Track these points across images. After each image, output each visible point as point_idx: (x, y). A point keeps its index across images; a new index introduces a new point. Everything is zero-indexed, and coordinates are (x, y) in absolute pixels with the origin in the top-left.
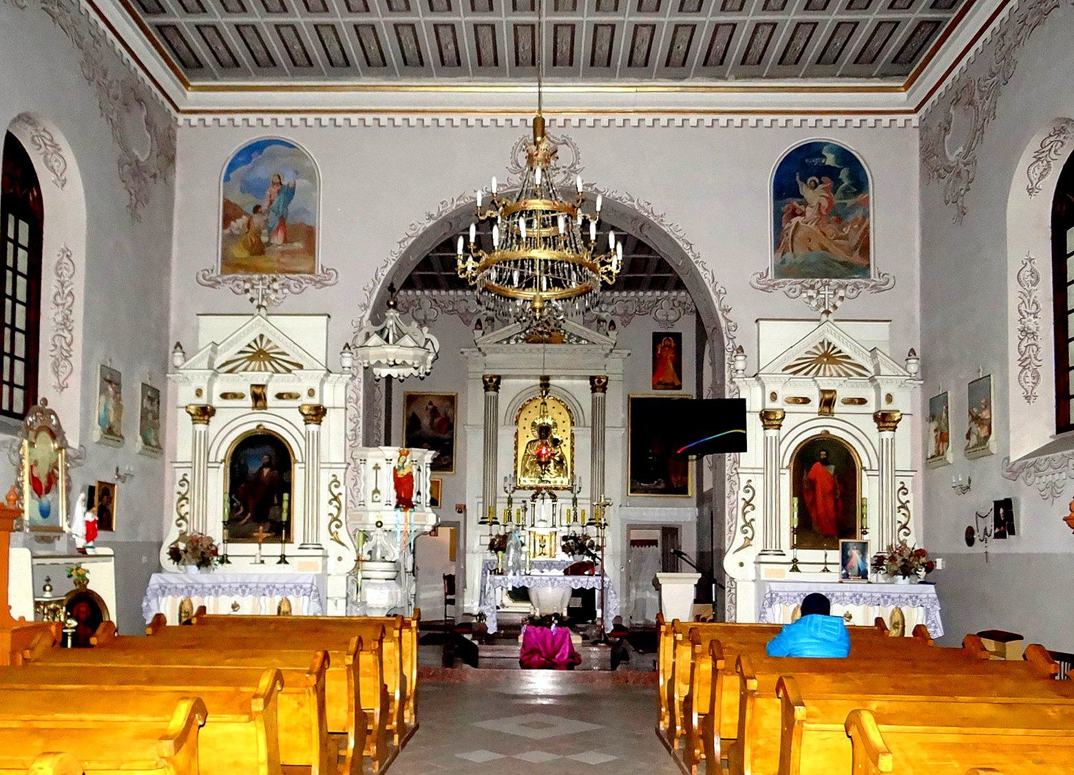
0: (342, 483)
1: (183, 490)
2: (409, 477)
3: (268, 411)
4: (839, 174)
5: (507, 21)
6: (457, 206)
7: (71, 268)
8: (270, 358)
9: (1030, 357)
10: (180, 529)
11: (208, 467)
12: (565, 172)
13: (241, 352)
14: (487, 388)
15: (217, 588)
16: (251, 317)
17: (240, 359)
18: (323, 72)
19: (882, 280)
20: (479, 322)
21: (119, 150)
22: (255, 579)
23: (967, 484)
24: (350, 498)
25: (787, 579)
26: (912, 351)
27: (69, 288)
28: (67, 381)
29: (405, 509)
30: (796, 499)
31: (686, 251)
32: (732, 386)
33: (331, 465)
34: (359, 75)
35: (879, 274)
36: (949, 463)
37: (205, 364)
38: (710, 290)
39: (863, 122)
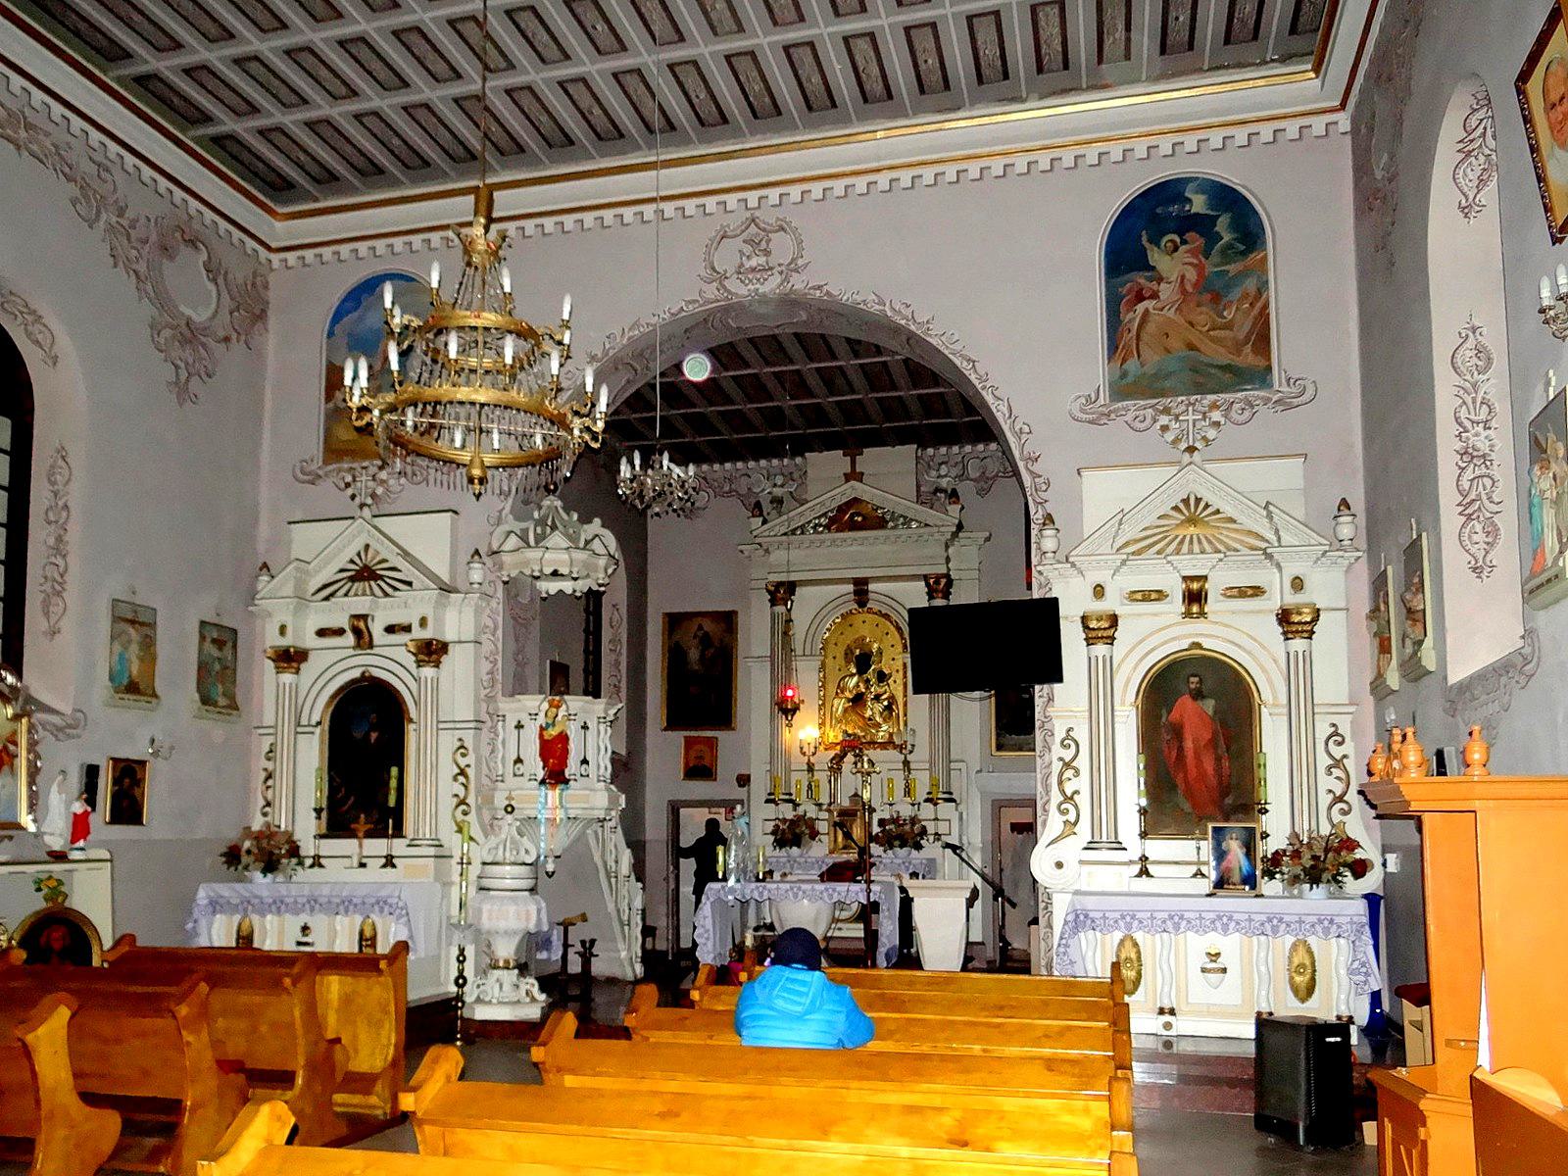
0: (470, 749)
1: (1068, 755)
2: (563, 738)
3: (376, 650)
6: (629, 339)
8: (377, 577)
9: (1479, 498)
10: (1065, 818)
11: (297, 733)
12: (781, 273)
13: (342, 571)
14: (773, 602)
16: (350, 521)
17: (340, 580)
18: (446, 173)
19: (1294, 390)
20: (758, 505)
21: (148, 310)
22: (326, 891)
24: (485, 770)
27: (63, 500)
29: (553, 786)
30: (1142, 757)
32: (1042, 579)
33: (454, 725)
38: (1006, 428)
39: (1254, 137)
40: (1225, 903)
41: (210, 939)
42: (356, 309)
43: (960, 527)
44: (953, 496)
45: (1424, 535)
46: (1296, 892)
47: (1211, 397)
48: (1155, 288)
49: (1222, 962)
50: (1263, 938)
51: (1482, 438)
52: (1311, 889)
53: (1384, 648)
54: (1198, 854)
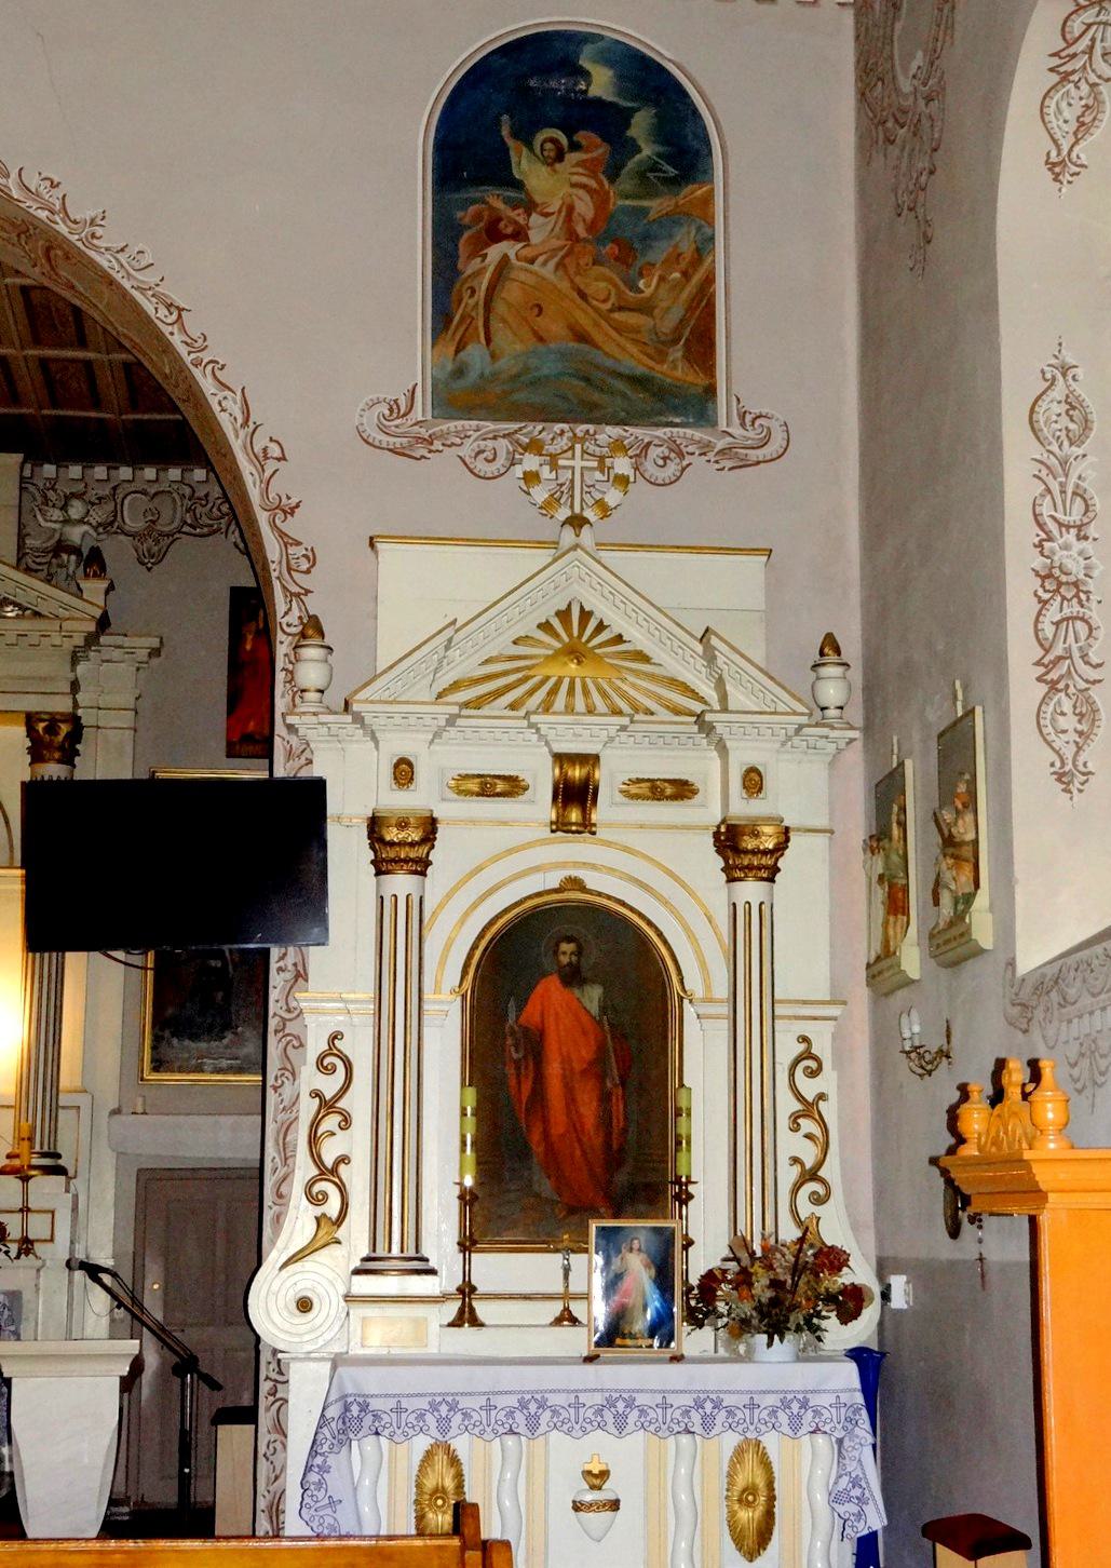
1: (330, 1085)
4: (628, 125)
10: (318, 1211)
19: (751, 434)
23: (940, 1041)
25: (432, 1350)
26: (830, 644)
30: (471, 1093)
31: (166, 330)
32: (294, 740)
35: (742, 416)
36: (913, 981)
38: (237, 445)
40: (618, 1375)
43: (103, 623)
44: (94, 562)
45: (979, 710)
46: (742, 1349)
47: (614, 431)
48: (521, 220)
49: (609, 1490)
51: (1074, 552)
52: (770, 1344)
53: (896, 904)
54: (566, 1277)
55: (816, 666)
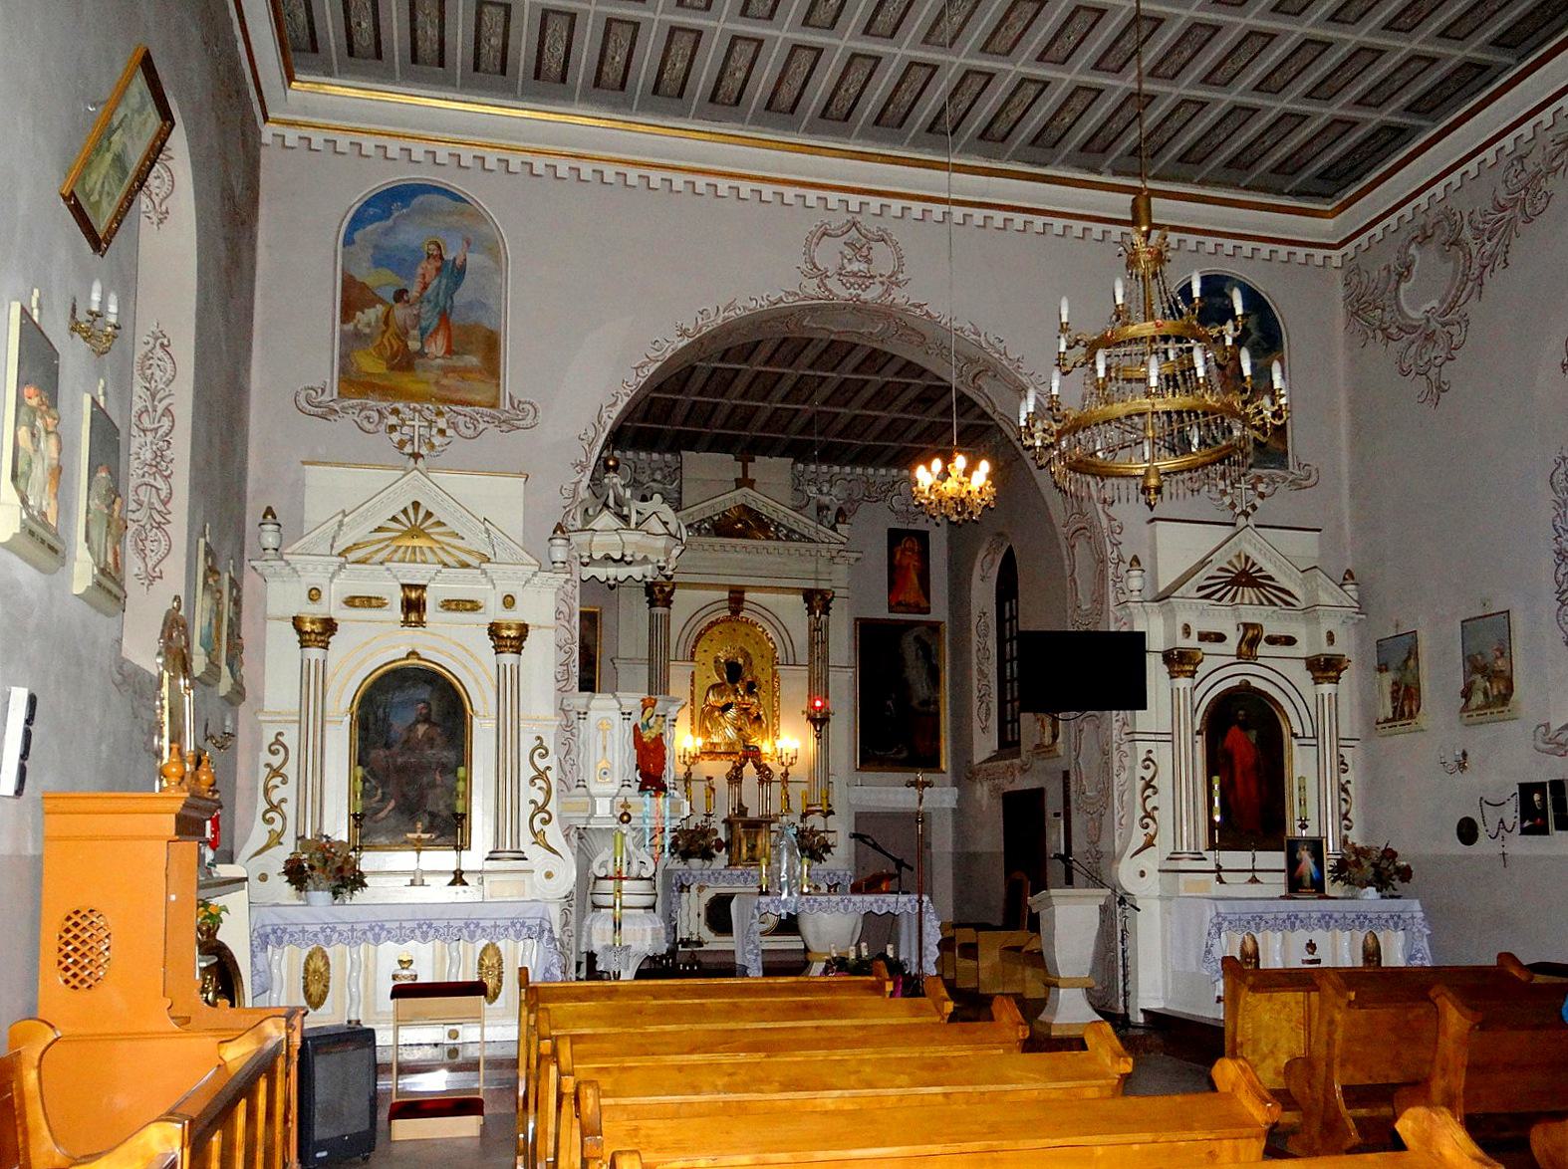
1: (276, 761)
5: (595, 12)
7: (169, 367)
10: (270, 827)
13: (380, 529)
15: (377, 929)
27: (165, 403)
28: (161, 566)
34: (631, 109)
36: (1058, 756)
37: (325, 548)
41: (1335, 956)
42: (381, 219)
50: (529, 941)
55: (550, 539)
